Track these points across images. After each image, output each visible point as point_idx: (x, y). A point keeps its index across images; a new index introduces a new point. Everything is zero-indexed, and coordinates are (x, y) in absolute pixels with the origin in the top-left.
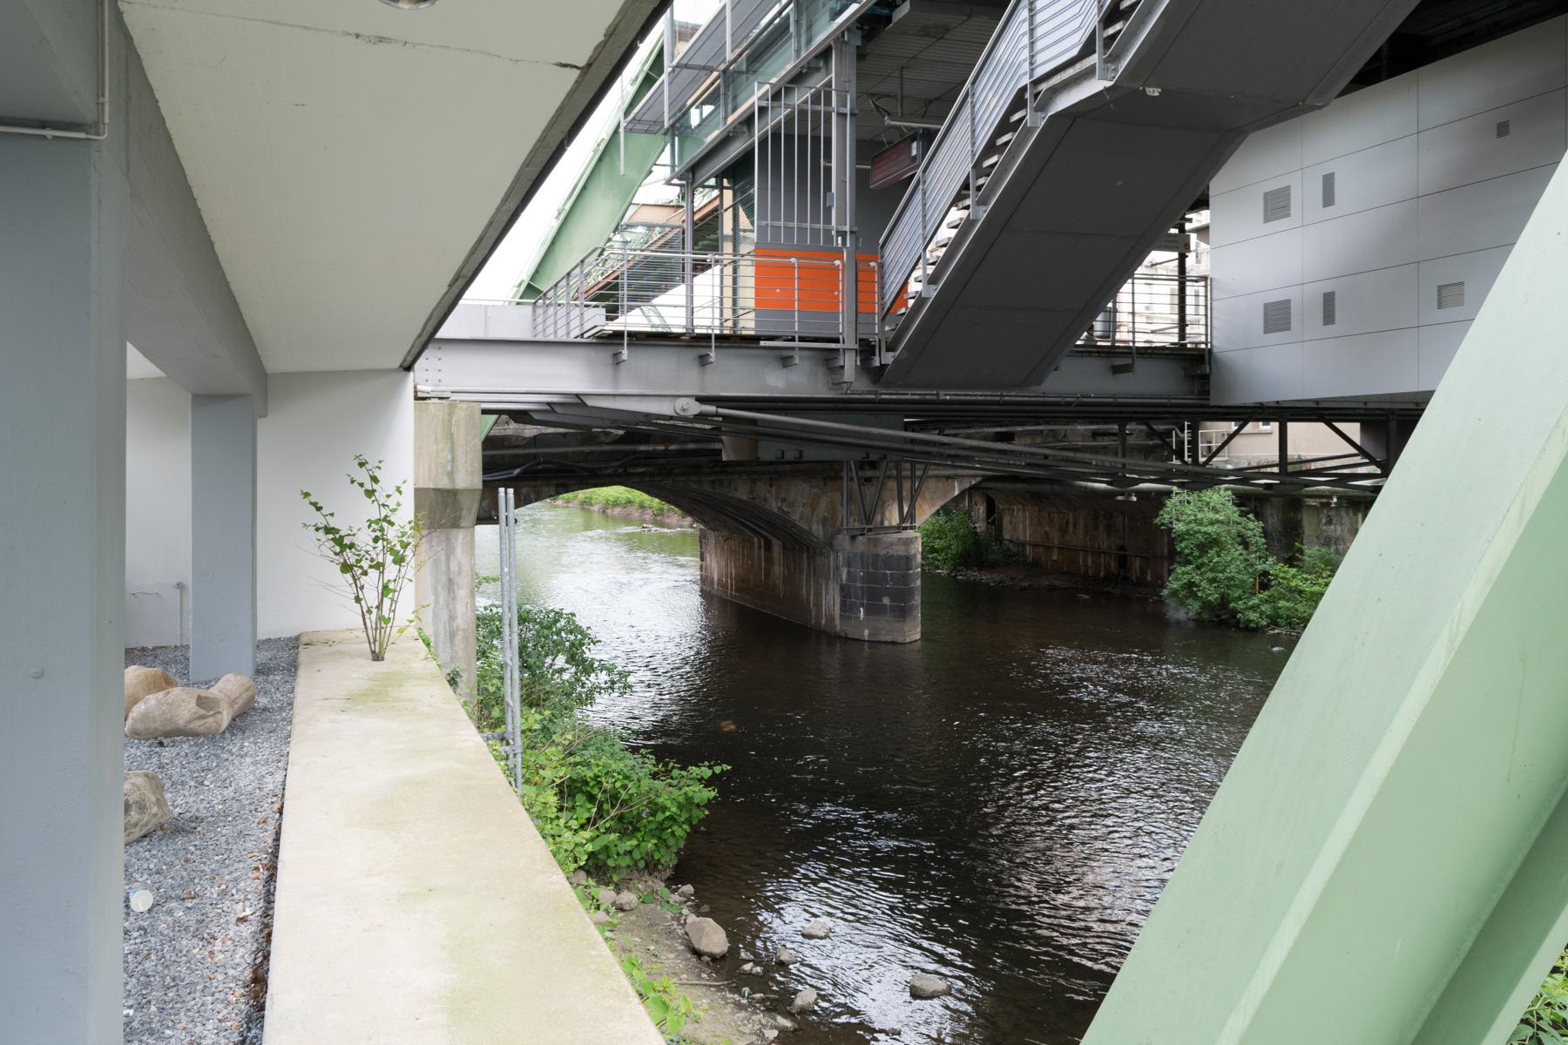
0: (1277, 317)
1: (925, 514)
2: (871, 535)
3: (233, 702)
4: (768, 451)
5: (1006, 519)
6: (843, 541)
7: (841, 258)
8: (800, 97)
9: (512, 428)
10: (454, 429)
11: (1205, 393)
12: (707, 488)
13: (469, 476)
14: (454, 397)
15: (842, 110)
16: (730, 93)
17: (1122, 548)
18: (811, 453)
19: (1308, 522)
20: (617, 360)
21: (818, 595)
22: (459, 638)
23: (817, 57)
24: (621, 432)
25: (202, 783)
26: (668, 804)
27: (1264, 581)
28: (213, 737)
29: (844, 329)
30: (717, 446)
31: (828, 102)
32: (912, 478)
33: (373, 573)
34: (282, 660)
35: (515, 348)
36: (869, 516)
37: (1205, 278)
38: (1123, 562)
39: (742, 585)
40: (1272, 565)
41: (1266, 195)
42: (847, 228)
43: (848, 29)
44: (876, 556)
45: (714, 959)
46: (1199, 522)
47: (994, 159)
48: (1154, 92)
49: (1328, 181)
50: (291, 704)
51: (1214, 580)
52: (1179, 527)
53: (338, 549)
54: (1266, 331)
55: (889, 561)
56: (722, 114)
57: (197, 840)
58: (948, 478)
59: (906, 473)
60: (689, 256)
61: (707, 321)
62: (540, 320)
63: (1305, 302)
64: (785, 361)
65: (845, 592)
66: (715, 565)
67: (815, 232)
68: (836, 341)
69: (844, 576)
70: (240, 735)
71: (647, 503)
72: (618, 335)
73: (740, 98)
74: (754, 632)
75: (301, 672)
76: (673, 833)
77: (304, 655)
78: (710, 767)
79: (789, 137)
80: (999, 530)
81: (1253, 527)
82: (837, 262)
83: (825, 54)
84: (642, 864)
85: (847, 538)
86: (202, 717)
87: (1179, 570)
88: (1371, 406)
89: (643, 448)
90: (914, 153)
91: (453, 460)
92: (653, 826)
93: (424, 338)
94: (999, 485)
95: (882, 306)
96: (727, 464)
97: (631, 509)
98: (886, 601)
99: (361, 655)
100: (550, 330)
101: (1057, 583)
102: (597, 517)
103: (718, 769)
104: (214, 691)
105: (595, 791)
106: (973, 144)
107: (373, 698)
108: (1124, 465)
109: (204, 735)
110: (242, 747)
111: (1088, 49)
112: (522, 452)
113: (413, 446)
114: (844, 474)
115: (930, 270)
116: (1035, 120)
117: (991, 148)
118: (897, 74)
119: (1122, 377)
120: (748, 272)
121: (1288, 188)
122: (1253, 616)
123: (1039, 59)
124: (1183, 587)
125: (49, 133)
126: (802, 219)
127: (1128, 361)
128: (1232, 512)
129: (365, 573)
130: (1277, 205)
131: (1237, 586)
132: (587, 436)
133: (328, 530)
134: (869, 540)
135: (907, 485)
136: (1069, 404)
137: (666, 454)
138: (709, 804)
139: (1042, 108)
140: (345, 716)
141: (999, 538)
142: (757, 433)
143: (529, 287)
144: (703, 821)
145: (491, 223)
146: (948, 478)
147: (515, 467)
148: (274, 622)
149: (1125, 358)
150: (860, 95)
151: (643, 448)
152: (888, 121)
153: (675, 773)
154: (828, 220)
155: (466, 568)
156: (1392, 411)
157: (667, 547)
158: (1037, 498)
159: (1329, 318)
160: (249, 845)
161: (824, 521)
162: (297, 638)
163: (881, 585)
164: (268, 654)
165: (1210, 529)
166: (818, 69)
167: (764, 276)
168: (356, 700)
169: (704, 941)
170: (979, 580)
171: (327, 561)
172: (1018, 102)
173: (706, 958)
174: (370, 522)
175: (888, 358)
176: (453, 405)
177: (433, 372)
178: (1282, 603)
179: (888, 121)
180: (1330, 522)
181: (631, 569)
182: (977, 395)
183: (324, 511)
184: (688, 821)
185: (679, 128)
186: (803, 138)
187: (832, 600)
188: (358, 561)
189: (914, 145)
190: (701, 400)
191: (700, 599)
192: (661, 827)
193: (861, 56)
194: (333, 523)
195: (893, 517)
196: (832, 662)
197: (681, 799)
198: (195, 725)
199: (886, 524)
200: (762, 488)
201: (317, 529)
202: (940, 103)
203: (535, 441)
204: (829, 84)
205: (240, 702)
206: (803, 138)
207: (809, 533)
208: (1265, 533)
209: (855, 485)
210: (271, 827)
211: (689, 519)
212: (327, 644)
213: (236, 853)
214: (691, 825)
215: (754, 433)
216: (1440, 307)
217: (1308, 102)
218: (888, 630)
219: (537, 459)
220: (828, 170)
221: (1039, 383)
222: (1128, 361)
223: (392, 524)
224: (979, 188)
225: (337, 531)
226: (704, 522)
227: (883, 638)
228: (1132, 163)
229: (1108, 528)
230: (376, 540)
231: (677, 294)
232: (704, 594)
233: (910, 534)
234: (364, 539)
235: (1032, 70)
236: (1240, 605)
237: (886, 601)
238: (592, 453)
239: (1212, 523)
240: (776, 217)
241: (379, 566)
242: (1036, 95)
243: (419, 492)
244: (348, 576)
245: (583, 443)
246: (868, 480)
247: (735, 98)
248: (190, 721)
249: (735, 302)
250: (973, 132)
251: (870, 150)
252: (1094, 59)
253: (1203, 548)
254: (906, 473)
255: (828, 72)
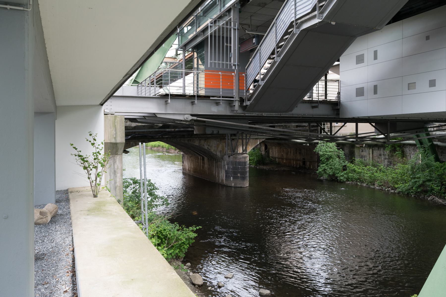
0: (360, 92)
1: (250, 149)
2: (235, 156)
3: (51, 213)
4: (209, 131)
5: (270, 151)
6: (226, 157)
7: (234, 72)
8: (221, 23)
9: (134, 124)
10: (116, 124)
11: (338, 114)
12: (186, 142)
13: (121, 139)
14: (116, 114)
15: (235, 28)
16: (198, 22)
17: (304, 159)
18: (222, 132)
19: (356, 152)
20: (166, 103)
21: (219, 173)
22: (118, 189)
23: (226, 12)
24: (161, 125)
25: (44, 241)
26: (183, 238)
27: (345, 168)
28: (45, 225)
29: (235, 94)
30: (190, 129)
31: (230, 25)
32: (246, 139)
33: (94, 170)
34: (64, 197)
35: (135, 99)
36: (234, 150)
37: (338, 81)
38: (304, 163)
39: (195, 170)
40: (347, 163)
41: (357, 56)
42: (236, 64)
43: (236, 3)
44: (236, 162)
45: (199, 286)
46: (326, 152)
47: (283, 43)
48: (333, 23)
49: (376, 53)
50: (70, 213)
51: (331, 168)
52: (321, 153)
53: (82, 162)
54: (357, 96)
55: (240, 163)
56: (195, 28)
57: (51, 267)
58: (256, 139)
59: (244, 137)
60: (184, 71)
61: (190, 91)
62: (140, 90)
63: (368, 87)
64: (217, 104)
65: (227, 172)
66: (187, 165)
67: (227, 65)
68: (233, 98)
69: (226, 168)
70: (54, 224)
71: (164, 146)
72: (167, 95)
73: (201, 24)
74: (198, 184)
75: (71, 202)
76: (184, 247)
77: (71, 196)
78: (195, 227)
79: (215, 36)
80: (269, 154)
81: (342, 153)
82: (233, 74)
83: (229, 10)
84: (175, 257)
85: (227, 157)
86: (42, 218)
87: (321, 165)
88: (383, 118)
89: (167, 130)
90: (254, 42)
91: (116, 133)
92: (178, 245)
93: (110, 95)
94: (269, 141)
95: (246, 88)
96: (196, 135)
97: (159, 148)
98: (239, 175)
99: (90, 195)
100: (144, 93)
101: (286, 169)
102: (149, 150)
103: (198, 228)
104: (44, 209)
105: (160, 235)
106: (276, 39)
107: (97, 210)
108: (310, 135)
109: (42, 224)
110: (56, 228)
111: (314, 10)
112: (131, 131)
113: (104, 129)
114: (227, 138)
115: (262, 76)
116: (296, 32)
117: (282, 40)
118: (249, 18)
119: (315, 109)
120: (202, 77)
121: (363, 54)
122: (342, 178)
123: (298, 13)
124: (323, 171)
125: (8, 7)
126: (223, 60)
127: (317, 105)
128: (335, 148)
129: (91, 170)
130: (360, 59)
131: (337, 170)
132: (152, 126)
133: (80, 156)
134: (234, 157)
135: (244, 141)
136: (300, 117)
137: (174, 132)
138: (195, 238)
139: (298, 28)
140: (89, 217)
141: (268, 156)
142: (205, 126)
143: (135, 80)
144: (192, 244)
145: (143, 56)
146: (256, 139)
147: (129, 136)
148: (61, 185)
149: (314, 104)
150: (240, 24)
151: (167, 130)
152: (247, 32)
153: (185, 229)
154: (230, 61)
155: (120, 167)
156: (389, 120)
157: (172, 160)
158: (279, 145)
159: (375, 92)
160: (64, 263)
161: (221, 152)
162: (67, 190)
163: (237, 170)
164: (59, 196)
165: (329, 153)
166: (227, 15)
167: (207, 77)
168: (91, 211)
169: (196, 281)
170: (263, 168)
171: (79, 166)
172: (291, 26)
173: (197, 286)
174: (94, 153)
175: (248, 103)
176: (116, 117)
177: (111, 106)
178: (350, 174)
179: (247, 32)
180: (362, 151)
181: (162, 166)
182: (274, 114)
183: (78, 150)
184: (189, 244)
185: (182, 34)
186: (223, 37)
187: (222, 175)
188: (89, 166)
189: (254, 39)
190: (192, 115)
191: (181, 175)
192: (180, 246)
193: (240, 12)
194: (81, 154)
195: (240, 150)
196: (223, 193)
197: (187, 237)
198: (40, 221)
199: (238, 152)
200: (202, 142)
201: (76, 156)
202: (265, 26)
203: (135, 128)
204: (230, 19)
205: (53, 212)
206: (223, 37)
207: (216, 155)
208: (345, 155)
209: (230, 141)
210: (70, 256)
211: (178, 150)
212: (78, 192)
213: (60, 267)
214: (189, 245)
215: (203, 125)
216: (408, 89)
217: (377, 28)
218: (239, 183)
219: (140, 133)
220: (230, 47)
221: (291, 111)
222: (317, 105)
223: (100, 154)
224: (278, 52)
225: (82, 156)
226: (184, 152)
227: (238, 186)
228: (320, 47)
229: (300, 153)
230: (95, 159)
231: (179, 82)
232: (184, 173)
233: (245, 155)
234: (91, 159)
235: (295, 16)
236: (338, 175)
237: (239, 175)
238: (152, 131)
239: (330, 152)
240: (215, 60)
241: (96, 167)
242: (297, 24)
243: (106, 144)
244: (86, 170)
245: (149, 128)
246: (233, 139)
247: (199, 24)
248: (38, 220)
249: (198, 85)
250: (276, 35)
251: (242, 41)
252: (316, 13)
253: (328, 159)
254: (244, 137)
255: (230, 16)
